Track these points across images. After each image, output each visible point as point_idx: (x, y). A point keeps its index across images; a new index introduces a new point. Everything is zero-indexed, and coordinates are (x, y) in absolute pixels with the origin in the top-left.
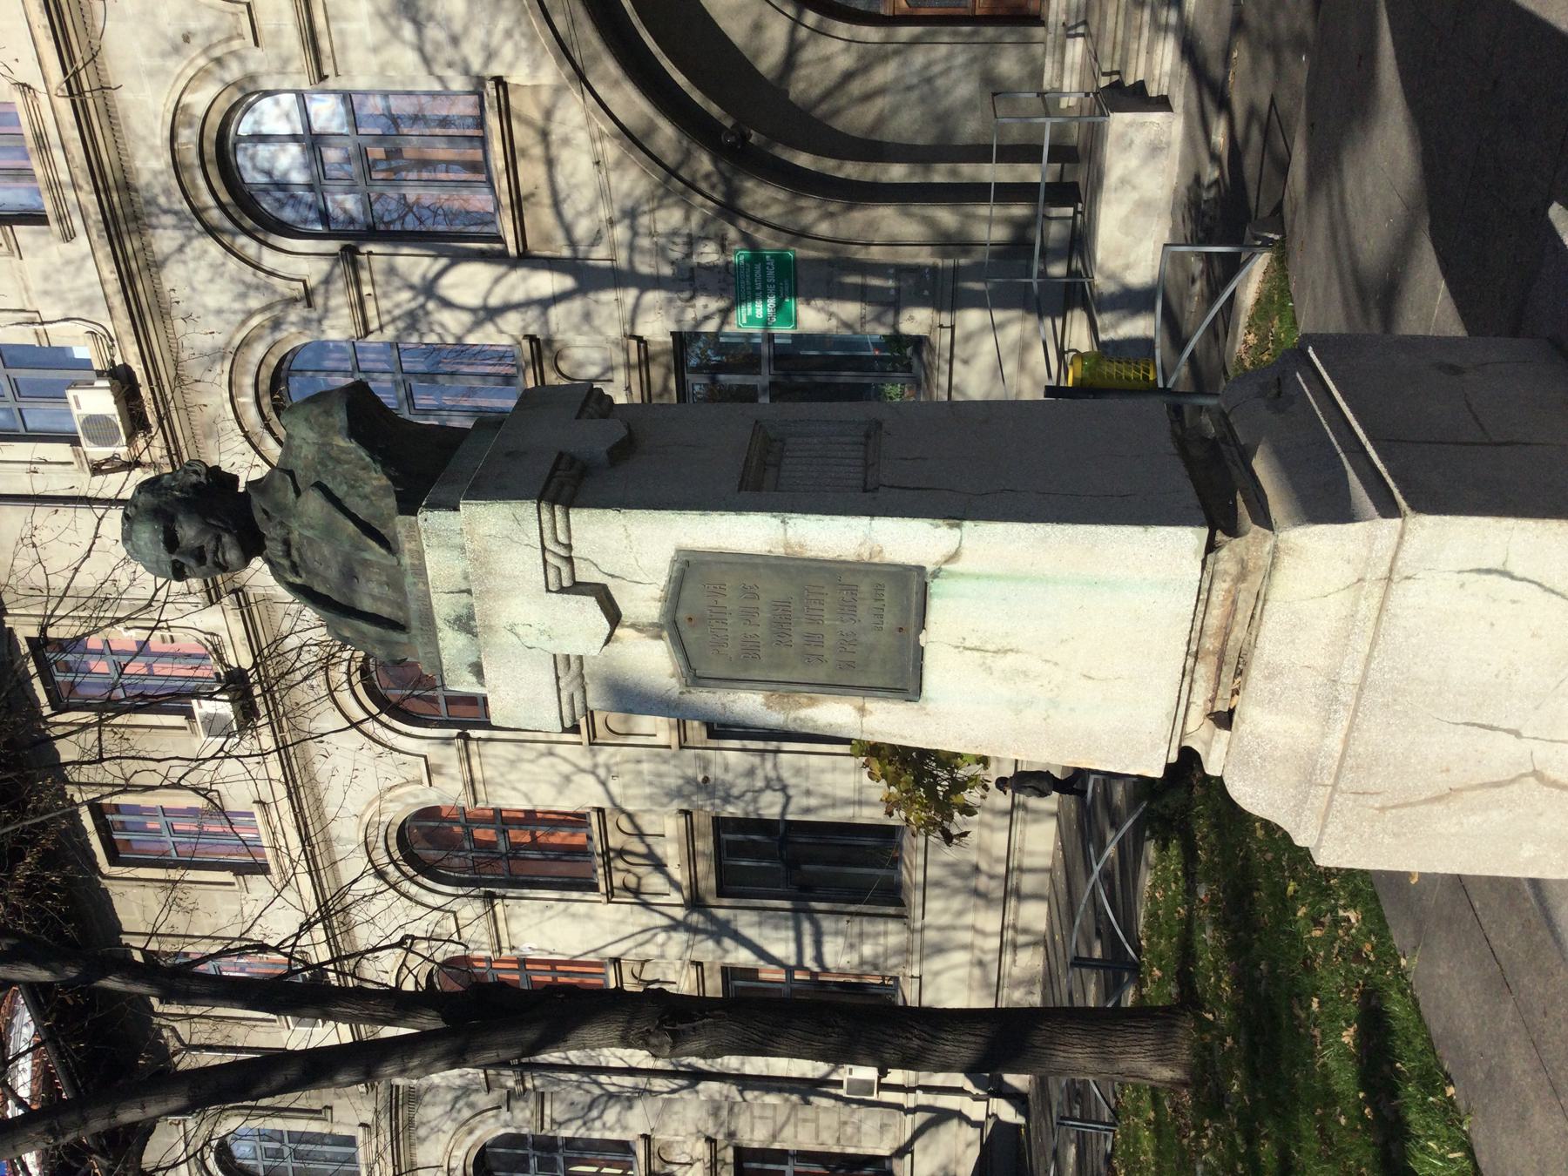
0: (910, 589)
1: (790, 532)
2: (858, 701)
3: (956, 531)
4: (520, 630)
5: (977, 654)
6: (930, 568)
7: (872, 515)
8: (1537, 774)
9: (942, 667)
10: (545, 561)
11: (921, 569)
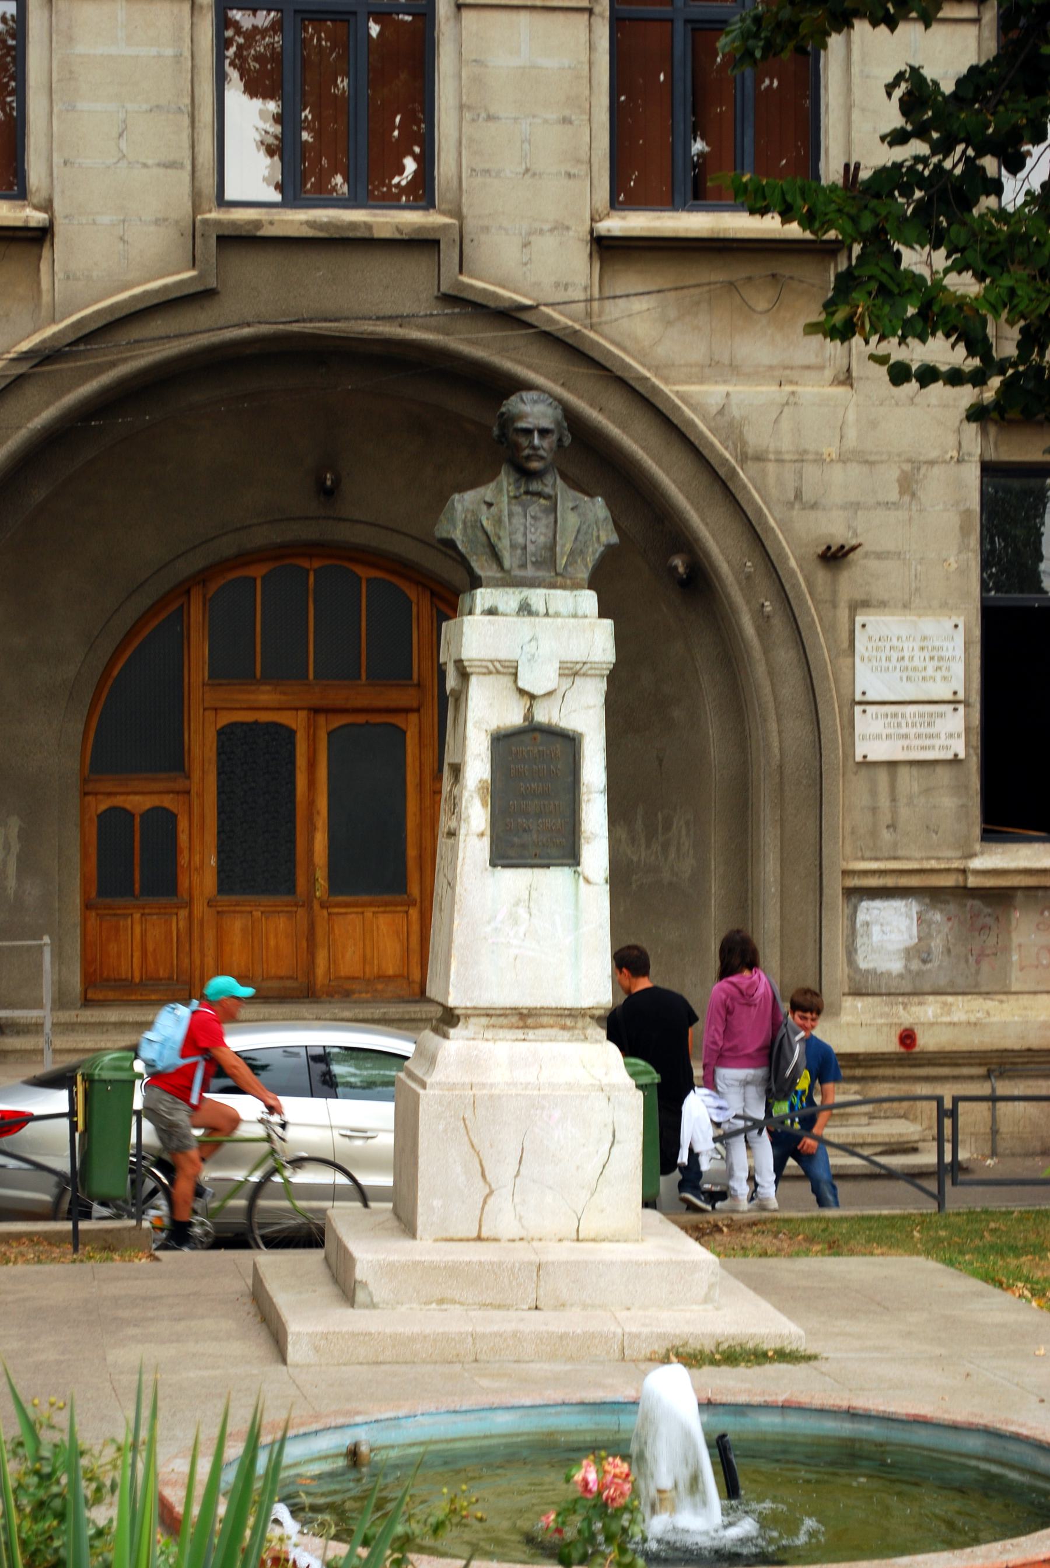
0: (569, 854)
1: (597, 795)
3: (603, 881)
4: (533, 643)
5: (527, 897)
6: (579, 869)
8: (491, 1192)
10: (577, 663)
11: (578, 864)
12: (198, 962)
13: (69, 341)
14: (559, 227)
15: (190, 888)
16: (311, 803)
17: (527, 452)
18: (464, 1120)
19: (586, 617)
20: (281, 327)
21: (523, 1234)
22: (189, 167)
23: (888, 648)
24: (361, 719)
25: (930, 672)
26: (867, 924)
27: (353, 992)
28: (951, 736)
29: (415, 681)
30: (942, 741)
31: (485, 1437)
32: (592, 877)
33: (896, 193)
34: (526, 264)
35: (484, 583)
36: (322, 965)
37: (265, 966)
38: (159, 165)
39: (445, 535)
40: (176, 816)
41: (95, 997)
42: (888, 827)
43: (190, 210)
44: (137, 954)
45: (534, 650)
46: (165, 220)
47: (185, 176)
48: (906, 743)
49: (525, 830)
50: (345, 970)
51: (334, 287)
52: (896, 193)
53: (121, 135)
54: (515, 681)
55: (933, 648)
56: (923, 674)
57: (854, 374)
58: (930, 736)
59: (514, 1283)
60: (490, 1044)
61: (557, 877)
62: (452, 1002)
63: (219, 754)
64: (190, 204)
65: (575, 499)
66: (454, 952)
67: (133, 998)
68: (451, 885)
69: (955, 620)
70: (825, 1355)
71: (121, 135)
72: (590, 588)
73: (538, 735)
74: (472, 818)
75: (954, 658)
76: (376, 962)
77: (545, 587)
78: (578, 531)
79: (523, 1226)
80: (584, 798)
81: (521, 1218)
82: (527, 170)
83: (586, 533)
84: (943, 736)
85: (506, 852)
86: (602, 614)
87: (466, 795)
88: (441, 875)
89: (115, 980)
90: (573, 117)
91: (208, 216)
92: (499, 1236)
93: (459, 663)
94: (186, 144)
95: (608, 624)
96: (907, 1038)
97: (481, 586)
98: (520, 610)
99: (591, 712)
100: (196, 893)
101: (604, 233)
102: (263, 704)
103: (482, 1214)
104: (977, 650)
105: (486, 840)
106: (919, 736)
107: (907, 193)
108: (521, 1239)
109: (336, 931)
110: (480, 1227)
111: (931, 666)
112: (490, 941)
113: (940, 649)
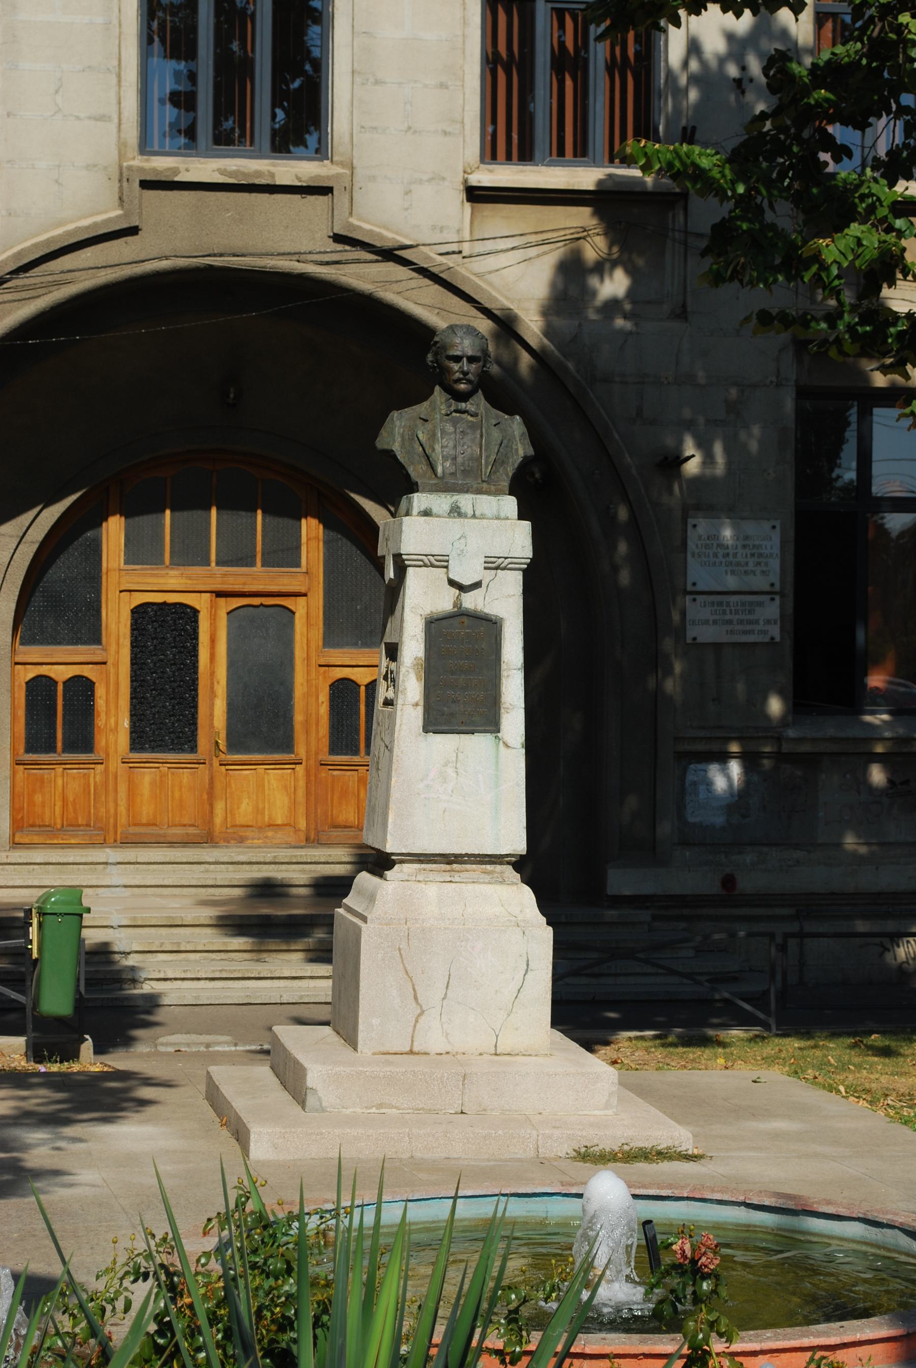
0: (488, 720)
2: (422, 703)
4: (462, 541)
5: (454, 759)
7: (526, 708)
9: (445, 744)
11: (499, 732)
12: (112, 811)
13: (10, 269)
14: (436, 178)
15: (107, 746)
16: (213, 674)
17: (458, 375)
18: (400, 950)
19: (507, 519)
20: (194, 260)
21: (449, 1049)
22: (116, 121)
23: (715, 545)
24: (256, 601)
25: (751, 567)
26: (694, 784)
27: (247, 839)
28: (768, 622)
29: (304, 570)
30: (760, 627)
31: (434, 1222)
32: (511, 742)
33: (761, 159)
34: (406, 209)
35: (420, 488)
36: (220, 815)
37: (170, 815)
38: (90, 118)
39: (386, 447)
40: (94, 683)
41: (22, 841)
42: (714, 700)
43: (117, 157)
44: (59, 804)
45: (463, 547)
46: (95, 166)
47: (113, 127)
48: (730, 627)
49: (453, 702)
50: (240, 820)
51: (241, 227)
52: (761, 159)
53: (57, 92)
54: (447, 573)
55: (754, 546)
56: (745, 568)
57: (689, 309)
58: (750, 622)
59: (443, 1090)
60: (422, 885)
61: (480, 742)
62: (389, 849)
63: (133, 630)
64: (116, 152)
65: (497, 417)
66: (392, 806)
67: (56, 842)
68: (389, 748)
69: (773, 523)
70: (709, 1154)
71: (57, 92)
72: (510, 494)
73: (465, 619)
74: (408, 690)
75: (772, 555)
76: (267, 813)
77: (472, 493)
78: (501, 445)
79: (449, 1042)
80: (504, 673)
81: (447, 1034)
82: (409, 128)
83: (507, 446)
84: (761, 622)
85: (437, 720)
86: (521, 517)
87: (403, 670)
88: (378, 738)
89: (40, 826)
90: (449, 83)
91: (132, 163)
92: (427, 1051)
93: (398, 557)
94: (114, 101)
95: (526, 525)
96: (729, 882)
97: (417, 491)
98: (451, 512)
99: (511, 600)
100: (111, 751)
101: (475, 184)
102: (169, 583)
103: (414, 1031)
104: (791, 548)
105: (420, 710)
106: (741, 622)
107: (770, 158)
108: (448, 1053)
109: (233, 785)
110: (412, 1041)
111: (751, 561)
112: (423, 796)
113: (759, 547)
